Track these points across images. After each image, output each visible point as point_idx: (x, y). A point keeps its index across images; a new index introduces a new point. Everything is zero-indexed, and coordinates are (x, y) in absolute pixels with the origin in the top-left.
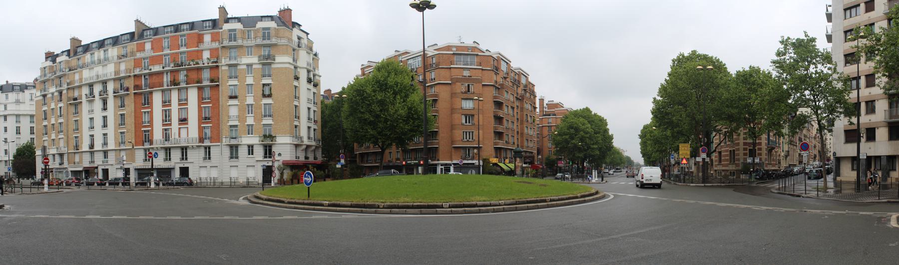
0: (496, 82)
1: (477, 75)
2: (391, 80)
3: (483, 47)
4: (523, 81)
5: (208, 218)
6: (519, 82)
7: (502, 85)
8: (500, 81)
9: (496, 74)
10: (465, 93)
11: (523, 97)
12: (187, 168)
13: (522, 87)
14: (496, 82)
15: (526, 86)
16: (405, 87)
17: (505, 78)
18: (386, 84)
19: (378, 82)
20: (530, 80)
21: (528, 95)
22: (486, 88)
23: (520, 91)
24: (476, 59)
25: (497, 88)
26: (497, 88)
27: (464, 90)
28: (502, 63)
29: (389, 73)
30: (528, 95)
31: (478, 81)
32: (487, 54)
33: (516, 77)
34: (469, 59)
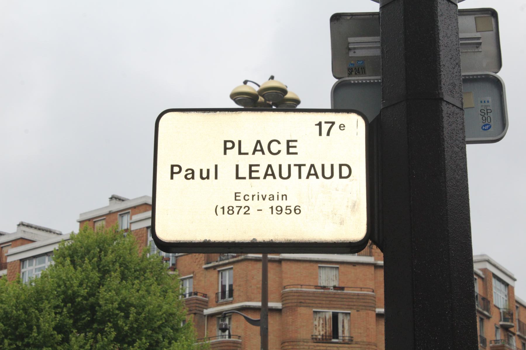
2: (108, 296)
15: (508, 315)
16: (150, 319)
18: (93, 308)
19: (69, 299)
27: (320, 331)
28: (495, 283)
29: (105, 272)
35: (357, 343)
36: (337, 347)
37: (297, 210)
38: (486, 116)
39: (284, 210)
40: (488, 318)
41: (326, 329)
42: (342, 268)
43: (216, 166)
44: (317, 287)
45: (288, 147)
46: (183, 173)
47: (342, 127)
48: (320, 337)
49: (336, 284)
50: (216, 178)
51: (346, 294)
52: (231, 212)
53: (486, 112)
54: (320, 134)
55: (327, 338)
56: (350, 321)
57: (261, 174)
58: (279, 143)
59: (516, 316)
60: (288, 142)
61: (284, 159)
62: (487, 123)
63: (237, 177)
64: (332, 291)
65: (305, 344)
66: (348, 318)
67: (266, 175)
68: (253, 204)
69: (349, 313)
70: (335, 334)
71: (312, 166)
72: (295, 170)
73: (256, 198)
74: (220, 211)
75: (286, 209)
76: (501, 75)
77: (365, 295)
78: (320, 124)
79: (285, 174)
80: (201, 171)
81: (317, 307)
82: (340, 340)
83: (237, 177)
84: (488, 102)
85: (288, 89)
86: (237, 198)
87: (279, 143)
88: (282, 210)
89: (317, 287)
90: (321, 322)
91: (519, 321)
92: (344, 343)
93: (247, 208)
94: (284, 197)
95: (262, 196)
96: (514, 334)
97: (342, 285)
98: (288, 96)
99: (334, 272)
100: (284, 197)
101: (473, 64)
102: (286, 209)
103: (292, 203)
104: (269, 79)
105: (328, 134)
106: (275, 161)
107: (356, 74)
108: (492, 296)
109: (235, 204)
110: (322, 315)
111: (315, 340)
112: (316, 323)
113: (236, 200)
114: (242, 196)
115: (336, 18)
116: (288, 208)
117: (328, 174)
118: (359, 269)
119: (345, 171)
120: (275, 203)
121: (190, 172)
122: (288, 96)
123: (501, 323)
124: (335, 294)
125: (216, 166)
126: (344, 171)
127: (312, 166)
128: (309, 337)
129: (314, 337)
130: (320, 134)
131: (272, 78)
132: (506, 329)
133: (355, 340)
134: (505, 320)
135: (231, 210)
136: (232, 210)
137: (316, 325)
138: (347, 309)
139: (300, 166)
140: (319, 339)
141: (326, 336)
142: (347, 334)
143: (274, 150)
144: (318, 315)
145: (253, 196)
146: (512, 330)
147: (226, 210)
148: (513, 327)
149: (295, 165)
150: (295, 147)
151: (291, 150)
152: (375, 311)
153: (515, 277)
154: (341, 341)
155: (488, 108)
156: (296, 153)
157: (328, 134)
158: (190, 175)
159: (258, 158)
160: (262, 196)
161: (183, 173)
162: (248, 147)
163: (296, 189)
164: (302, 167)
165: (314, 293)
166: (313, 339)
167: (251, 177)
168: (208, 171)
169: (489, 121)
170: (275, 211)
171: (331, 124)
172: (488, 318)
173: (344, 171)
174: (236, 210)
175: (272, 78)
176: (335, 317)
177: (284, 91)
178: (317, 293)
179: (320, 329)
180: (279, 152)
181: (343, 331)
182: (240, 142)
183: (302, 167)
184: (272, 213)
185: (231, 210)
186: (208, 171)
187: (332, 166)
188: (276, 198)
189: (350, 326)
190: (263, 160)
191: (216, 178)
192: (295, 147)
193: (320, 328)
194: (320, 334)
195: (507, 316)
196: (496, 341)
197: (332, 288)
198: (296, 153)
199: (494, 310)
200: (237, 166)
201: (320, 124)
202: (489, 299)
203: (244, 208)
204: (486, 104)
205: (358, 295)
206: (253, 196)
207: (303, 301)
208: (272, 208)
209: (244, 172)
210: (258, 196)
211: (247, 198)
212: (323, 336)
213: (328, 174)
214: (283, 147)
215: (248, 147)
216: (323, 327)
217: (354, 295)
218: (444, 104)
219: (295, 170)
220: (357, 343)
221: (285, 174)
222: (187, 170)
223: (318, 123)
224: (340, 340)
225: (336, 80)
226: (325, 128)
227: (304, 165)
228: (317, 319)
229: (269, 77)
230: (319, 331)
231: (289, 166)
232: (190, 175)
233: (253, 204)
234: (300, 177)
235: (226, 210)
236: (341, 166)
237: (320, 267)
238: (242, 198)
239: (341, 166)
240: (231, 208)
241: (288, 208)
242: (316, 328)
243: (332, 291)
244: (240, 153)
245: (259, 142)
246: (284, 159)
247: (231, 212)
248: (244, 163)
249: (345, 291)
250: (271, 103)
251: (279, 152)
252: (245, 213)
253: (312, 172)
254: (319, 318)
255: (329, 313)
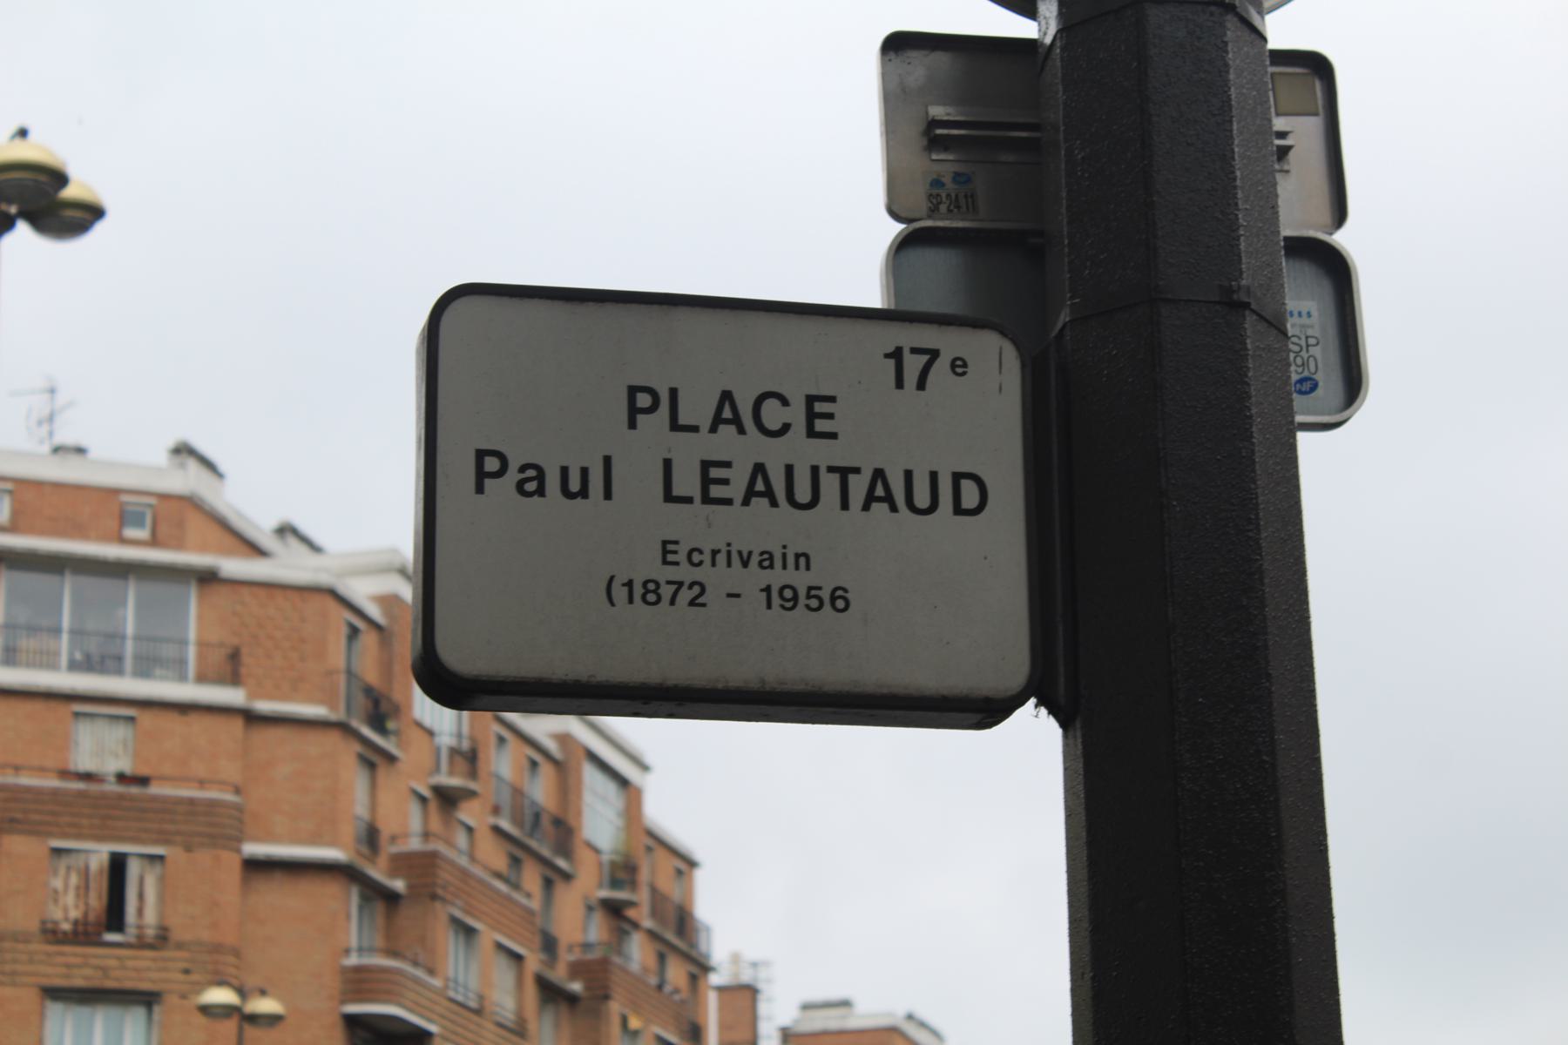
0: (371, 838)
1: (201, 769)
3: (250, 500)
4: (600, 823)
5: (960, 224)
6: (564, 831)
7: (421, 866)
8: (409, 826)
9: (375, 760)
10: (84, 934)
11: (598, 973)
12: (1286, 239)
13: (588, 884)
14: (371, 838)
15: (623, 872)
17: (447, 799)
20: (661, 811)
21: (638, 952)
22: (276, 895)
23: (575, 923)
24: (193, 618)
25: (376, 894)
26: (376, 894)
27: (68, 908)
28: (590, 775)
30: (638, 952)
31: (210, 826)
32: (290, 566)
33: (541, 790)
34: (130, 612)
35: (180, 946)
36: (118, 958)
37: (839, 599)
38: (1304, 354)
39: (802, 600)
40: (567, 877)
41: (87, 904)
42: (146, 718)
43: (607, 461)
44: (65, 774)
45: (811, 416)
46: (512, 476)
47: (959, 366)
48: (66, 927)
49: (125, 765)
50: (608, 495)
51: (154, 799)
52: (651, 597)
53: (1303, 343)
54: (900, 384)
55: (90, 929)
56: (162, 880)
57: (736, 490)
58: (785, 402)
59: (644, 875)
60: (811, 400)
61: (800, 451)
62: (1306, 374)
63: (669, 497)
64: (112, 787)
65: (21, 946)
66: (158, 868)
67: (750, 494)
68: (718, 578)
69: (161, 858)
70: (114, 915)
71: (879, 474)
72: (830, 484)
73: (722, 558)
74: (620, 593)
75: (809, 597)
76: (1342, 239)
77: (213, 804)
78: (897, 355)
79: (803, 494)
80: (564, 471)
81: (65, 836)
82: (130, 935)
83: (669, 497)
84: (1309, 315)
85: (73, 171)
86: (670, 558)
87: (785, 402)
88: (795, 598)
89: (65, 774)
90: (74, 880)
91: (654, 890)
92: (141, 944)
93: (697, 589)
94: (802, 561)
95: (740, 553)
96: (636, 925)
97: (144, 771)
98: (70, 192)
99: (121, 732)
100: (802, 561)
101: (1297, 213)
102: (809, 597)
103: (823, 576)
104: (13, 137)
105: (921, 385)
106: (775, 455)
107: (950, 211)
108: (579, 813)
109: (665, 574)
110: (78, 861)
111: (52, 934)
112: (58, 883)
113: (665, 562)
114: (683, 550)
115: (897, 44)
116: (813, 592)
117: (922, 500)
118: (198, 723)
119: (970, 497)
120: (777, 578)
121: (531, 473)
122: (70, 192)
123: (605, 893)
124: (121, 797)
125: (607, 461)
126: (964, 494)
127: (879, 474)
128: (33, 926)
129: (49, 926)
130: (900, 384)
131: (23, 133)
132: (614, 910)
133: (177, 935)
134: (615, 883)
135: (651, 592)
136: (655, 592)
137: (56, 891)
138: (156, 842)
139: (844, 473)
140: (65, 933)
141: (86, 924)
142: (151, 917)
143: (772, 423)
144: (63, 863)
145: (715, 553)
146: (631, 913)
147: (638, 590)
148: (631, 904)
149: (831, 469)
150: (830, 416)
151: (820, 425)
152: (238, 851)
153: (649, 759)
154: (132, 940)
155: (1310, 332)
156: (833, 436)
157: (921, 385)
158: (533, 482)
159: (725, 443)
160: (740, 553)
161: (512, 476)
162: (696, 409)
163: (847, 542)
164: (852, 478)
165: (55, 793)
166: (44, 931)
167: (707, 499)
168: (584, 472)
169: (1313, 369)
170: (776, 600)
171: (925, 358)
172: (567, 877)
173: (964, 494)
174: (667, 592)
175: (23, 133)
176: (118, 866)
177: (59, 178)
178: (65, 792)
179: (70, 904)
180: (786, 428)
181: (140, 912)
182: (673, 393)
183: (852, 478)
184: (769, 606)
185: (651, 592)
186: (584, 472)
187: (934, 476)
188: (778, 563)
189: (161, 899)
190: (741, 450)
191: (608, 495)
192: (830, 416)
193: (70, 899)
194: (66, 919)
195: (621, 875)
196: (586, 946)
197: (112, 779)
198: (833, 436)
199: (584, 855)
200: (668, 464)
201: (897, 355)
202: (572, 821)
203: (690, 587)
204: (1305, 320)
205: (191, 802)
206: (715, 553)
207: (19, 816)
208: (768, 589)
209: (687, 483)
210: (729, 553)
211: (696, 558)
212: (76, 923)
213: (922, 500)
214: (796, 414)
215: (696, 409)
216: (78, 896)
217: (180, 801)
218: (1250, 321)
219: (830, 484)
220: (180, 946)
221: (803, 494)
222: (523, 469)
223: (891, 349)
224: (130, 935)
225: (899, 227)
226: (913, 364)
227: (857, 471)
228: (62, 871)
229: (13, 128)
230: (66, 910)
231: (815, 470)
232: (533, 482)
233: (718, 578)
234: (845, 505)
235: (638, 590)
236: (957, 477)
237: (77, 715)
238: (681, 557)
239: (957, 477)
240: (651, 586)
241: (813, 592)
242: (56, 901)
243: (112, 787)
244: (675, 426)
245: (727, 396)
246: (800, 451)
247: (651, 597)
248: (688, 454)
249: (155, 789)
250: (13, 210)
251: (786, 428)
252: (692, 603)
253: (879, 493)
254: (69, 868)
255: (98, 854)
